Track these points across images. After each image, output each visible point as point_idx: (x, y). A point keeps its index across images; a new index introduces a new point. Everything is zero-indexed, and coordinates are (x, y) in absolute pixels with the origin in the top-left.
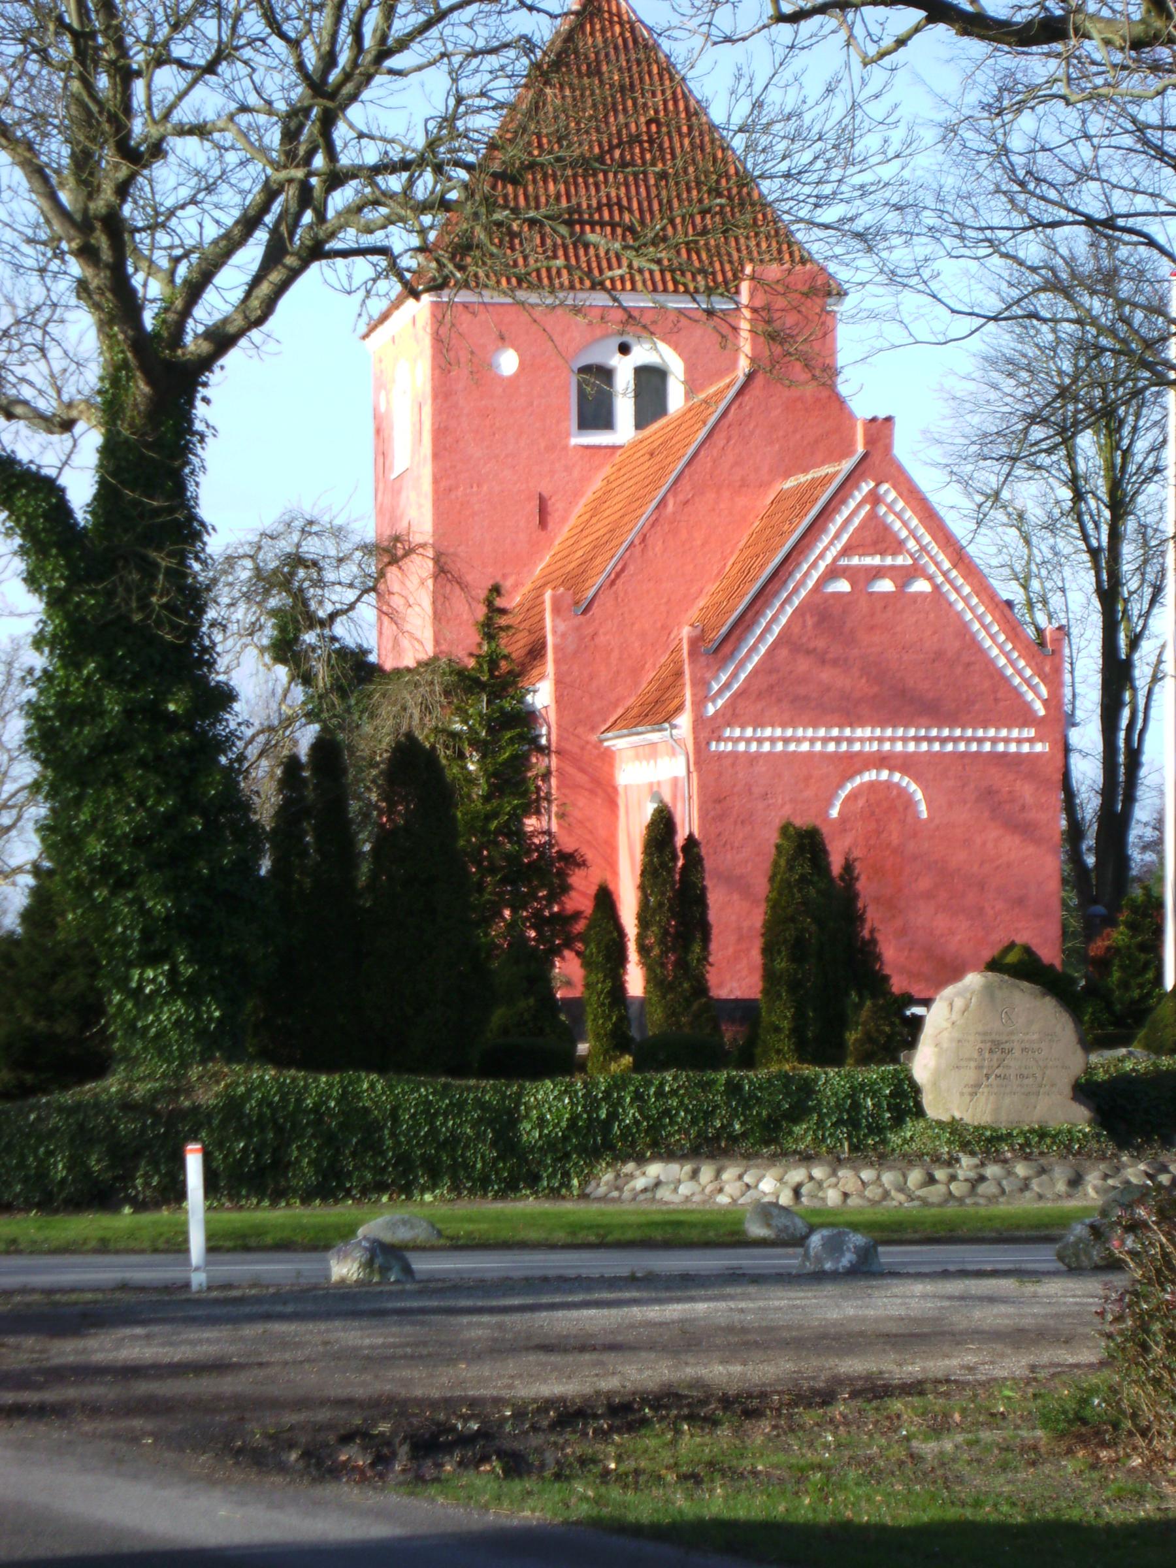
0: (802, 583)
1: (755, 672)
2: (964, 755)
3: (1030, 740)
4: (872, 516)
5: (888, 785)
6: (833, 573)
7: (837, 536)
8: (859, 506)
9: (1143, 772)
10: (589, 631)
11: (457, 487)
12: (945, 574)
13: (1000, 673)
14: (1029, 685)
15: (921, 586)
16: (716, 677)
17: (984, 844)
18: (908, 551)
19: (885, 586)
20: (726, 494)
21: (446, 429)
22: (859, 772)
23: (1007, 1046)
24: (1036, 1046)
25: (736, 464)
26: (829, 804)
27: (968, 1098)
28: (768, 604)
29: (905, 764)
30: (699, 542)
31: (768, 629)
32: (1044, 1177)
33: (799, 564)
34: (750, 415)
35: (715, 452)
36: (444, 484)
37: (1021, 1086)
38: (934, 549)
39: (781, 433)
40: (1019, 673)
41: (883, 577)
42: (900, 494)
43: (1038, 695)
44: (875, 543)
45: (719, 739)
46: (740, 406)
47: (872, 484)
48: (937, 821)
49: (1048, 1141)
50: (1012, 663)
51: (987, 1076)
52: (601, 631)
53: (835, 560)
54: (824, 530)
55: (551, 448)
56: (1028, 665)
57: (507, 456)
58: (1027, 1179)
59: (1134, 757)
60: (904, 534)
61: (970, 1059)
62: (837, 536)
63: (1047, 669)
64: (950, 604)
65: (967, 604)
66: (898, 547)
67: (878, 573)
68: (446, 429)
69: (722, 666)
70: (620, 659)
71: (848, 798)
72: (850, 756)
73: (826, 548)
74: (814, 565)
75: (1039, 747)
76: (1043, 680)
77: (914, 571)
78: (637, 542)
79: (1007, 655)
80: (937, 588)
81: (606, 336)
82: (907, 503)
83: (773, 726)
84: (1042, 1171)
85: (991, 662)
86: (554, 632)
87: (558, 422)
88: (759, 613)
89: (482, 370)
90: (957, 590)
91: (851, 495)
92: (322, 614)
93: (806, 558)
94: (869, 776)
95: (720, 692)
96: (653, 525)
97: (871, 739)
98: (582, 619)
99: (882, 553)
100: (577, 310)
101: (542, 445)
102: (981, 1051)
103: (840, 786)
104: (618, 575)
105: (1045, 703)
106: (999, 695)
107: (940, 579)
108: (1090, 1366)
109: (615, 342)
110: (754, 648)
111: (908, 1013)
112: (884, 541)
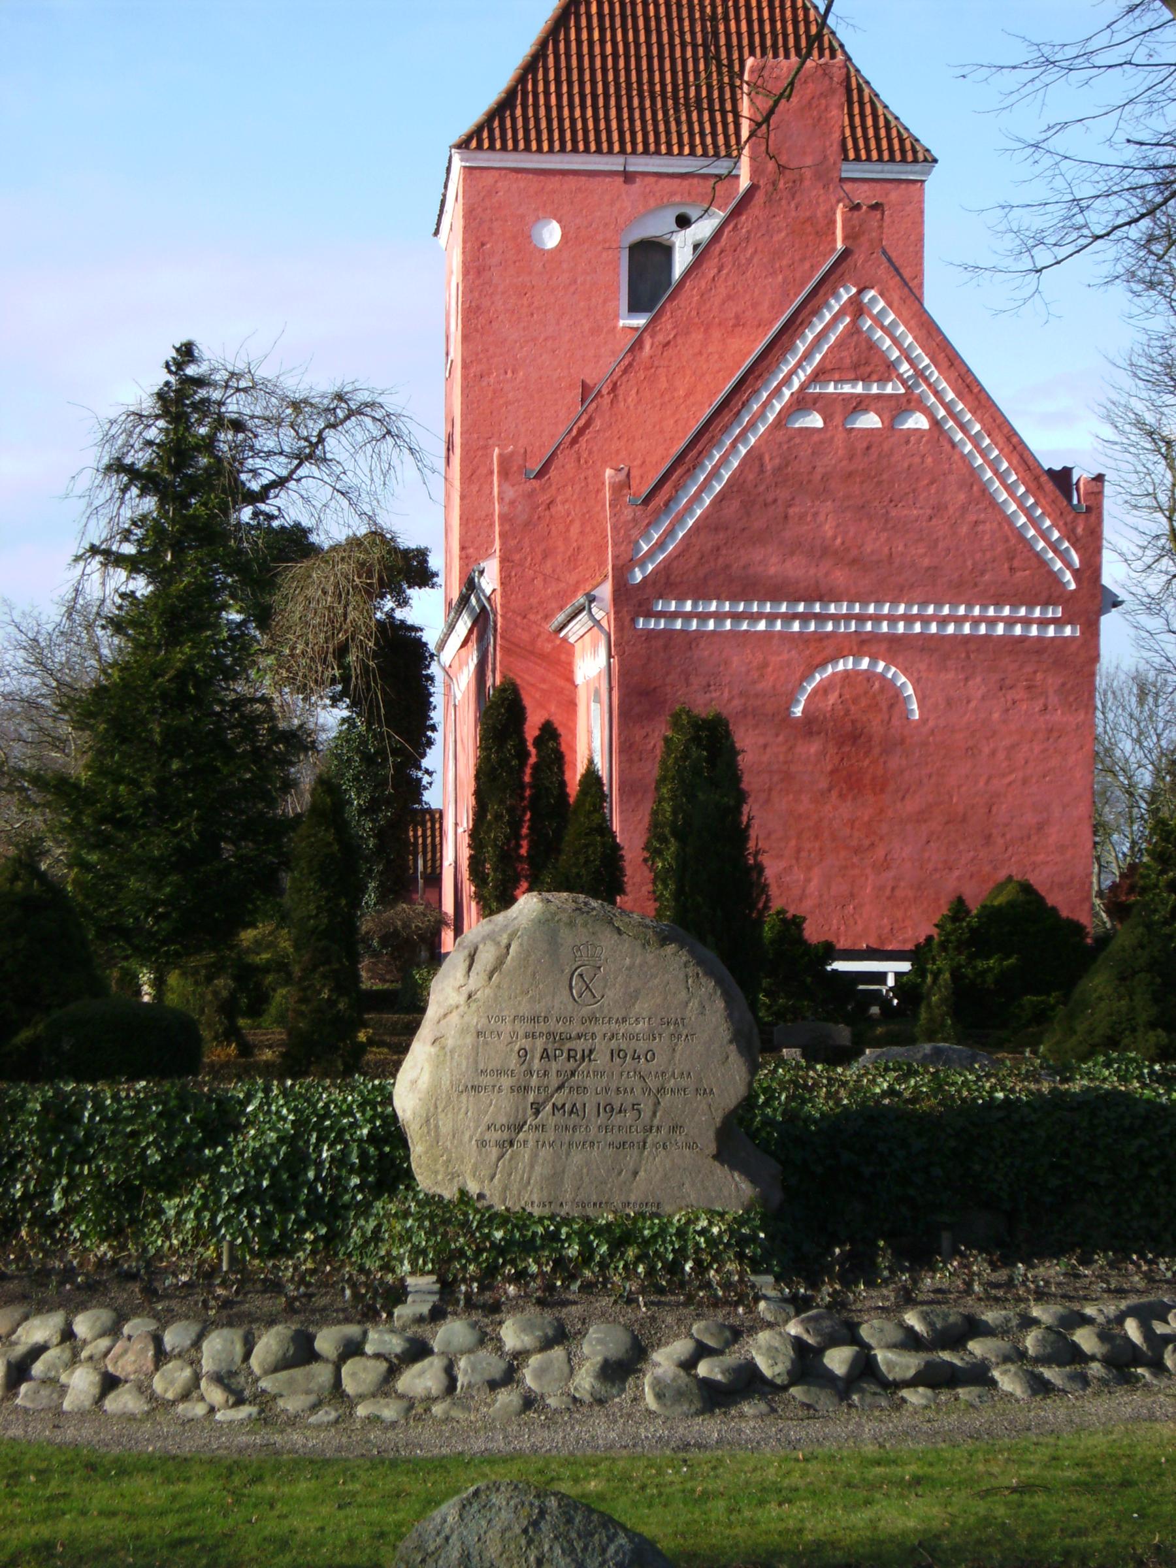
0: (761, 414)
1: (696, 528)
2: (967, 639)
3: (1057, 622)
4: (854, 330)
5: (869, 675)
6: (801, 402)
7: (807, 356)
8: (836, 318)
10: (544, 498)
11: (489, 374)
12: (948, 407)
13: (1019, 534)
14: (1056, 551)
15: (918, 421)
16: (645, 534)
17: (993, 753)
18: (900, 376)
19: (870, 421)
20: (716, 334)
21: (478, 307)
22: (834, 659)
23: (580, 1045)
24: (642, 1046)
25: (729, 297)
26: (792, 700)
27: (494, 1152)
28: (715, 442)
29: (894, 648)
30: (682, 393)
31: (715, 474)
32: (558, 1352)
33: (756, 392)
34: (748, 239)
35: (703, 284)
36: (474, 369)
38: (935, 375)
39: (785, 262)
40: (1044, 535)
41: (866, 410)
42: (890, 304)
43: (1068, 564)
44: (856, 366)
45: (649, 614)
46: (735, 228)
47: (854, 290)
48: (931, 723)
49: (631, 1253)
50: (1034, 522)
51: (537, 1110)
52: (559, 499)
53: (803, 387)
54: (790, 348)
55: (596, 331)
56: (1055, 525)
57: (546, 339)
58: (521, 1355)
60: (895, 354)
61: (500, 1072)
62: (807, 356)
63: (1079, 530)
64: (954, 445)
65: (977, 446)
66: (888, 370)
67: (860, 404)
68: (478, 307)
69: (653, 522)
70: (582, 533)
71: (815, 692)
72: (821, 638)
73: (793, 372)
74: (777, 392)
75: (1068, 631)
76: (1073, 545)
77: (908, 403)
78: (605, 391)
79: (1028, 512)
80: (936, 423)
81: (661, 206)
82: (898, 314)
83: (718, 598)
84: (559, 1336)
85: (1009, 520)
86: (501, 499)
87: (605, 302)
88: (705, 453)
89: (523, 241)
90: (963, 427)
91: (826, 304)
92: (255, 486)
93: (766, 384)
94: (845, 665)
95: (651, 554)
96: (625, 371)
97: (848, 617)
98: (536, 484)
99: (866, 379)
100: (628, 177)
101: (587, 327)
102: (523, 1054)
103: (807, 676)
104: (581, 432)
105: (1076, 573)
106: (1016, 564)
107: (941, 413)
109: (669, 218)
110: (697, 498)
111: (829, 968)
112: (867, 363)
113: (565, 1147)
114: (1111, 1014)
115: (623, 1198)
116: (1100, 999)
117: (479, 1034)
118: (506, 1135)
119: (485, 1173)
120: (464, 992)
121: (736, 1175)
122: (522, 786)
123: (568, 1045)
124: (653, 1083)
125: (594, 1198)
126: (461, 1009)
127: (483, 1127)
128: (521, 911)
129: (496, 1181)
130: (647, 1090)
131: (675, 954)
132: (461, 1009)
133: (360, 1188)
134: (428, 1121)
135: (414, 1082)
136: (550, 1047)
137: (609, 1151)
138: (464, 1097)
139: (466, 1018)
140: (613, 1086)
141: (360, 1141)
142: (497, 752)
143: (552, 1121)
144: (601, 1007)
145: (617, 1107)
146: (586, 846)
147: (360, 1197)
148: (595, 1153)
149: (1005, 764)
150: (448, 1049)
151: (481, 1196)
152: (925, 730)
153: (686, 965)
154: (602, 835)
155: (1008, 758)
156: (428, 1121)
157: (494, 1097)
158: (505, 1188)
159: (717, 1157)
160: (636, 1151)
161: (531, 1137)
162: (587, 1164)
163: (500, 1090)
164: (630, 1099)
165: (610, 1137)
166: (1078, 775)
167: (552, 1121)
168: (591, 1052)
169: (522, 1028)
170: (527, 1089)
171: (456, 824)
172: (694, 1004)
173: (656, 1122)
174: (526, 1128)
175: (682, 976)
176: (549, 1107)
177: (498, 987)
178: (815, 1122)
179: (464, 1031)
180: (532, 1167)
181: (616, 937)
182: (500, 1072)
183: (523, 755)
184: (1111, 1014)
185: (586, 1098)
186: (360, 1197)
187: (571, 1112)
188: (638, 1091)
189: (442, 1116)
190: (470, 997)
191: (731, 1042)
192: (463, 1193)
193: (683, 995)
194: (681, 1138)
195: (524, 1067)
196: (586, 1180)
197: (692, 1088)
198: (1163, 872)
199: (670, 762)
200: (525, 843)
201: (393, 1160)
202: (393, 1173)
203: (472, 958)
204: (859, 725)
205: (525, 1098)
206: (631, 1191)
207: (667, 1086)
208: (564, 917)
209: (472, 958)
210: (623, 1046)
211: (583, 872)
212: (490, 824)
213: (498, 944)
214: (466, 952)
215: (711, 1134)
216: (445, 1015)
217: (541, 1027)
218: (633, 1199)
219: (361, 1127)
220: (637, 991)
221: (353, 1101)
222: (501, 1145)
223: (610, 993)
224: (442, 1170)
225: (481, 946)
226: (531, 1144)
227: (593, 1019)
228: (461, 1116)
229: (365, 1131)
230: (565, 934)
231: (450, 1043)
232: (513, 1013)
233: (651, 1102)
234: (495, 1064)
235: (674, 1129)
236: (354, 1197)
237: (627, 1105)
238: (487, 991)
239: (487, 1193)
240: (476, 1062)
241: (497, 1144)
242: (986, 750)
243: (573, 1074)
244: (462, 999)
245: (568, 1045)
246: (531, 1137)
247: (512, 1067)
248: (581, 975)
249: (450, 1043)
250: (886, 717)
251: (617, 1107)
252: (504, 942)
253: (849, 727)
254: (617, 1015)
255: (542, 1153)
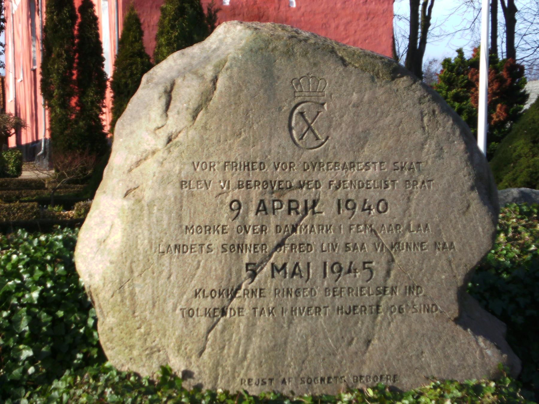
9: (430, 28)
17: (337, 27)
27: (204, 322)
37: (335, 292)
48: (302, 10)
59: (427, 20)
61: (209, 229)
108: (363, 98)
113: (286, 315)
114: (529, 167)
115: (355, 371)
116: (520, 156)
117: (182, 184)
118: (217, 303)
119: (192, 347)
120: (163, 135)
121: (481, 339)
122: (73, 37)
123: (289, 196)
124: (386, 238)
125: (322, 373)
126: (160, 155)
127: (190, 293)
128: (221, 41)
129: (205, 355)
130: (379, 245)
131: (408, 88)
132: (160, 155)
133: (31, 361)
134: (121, 287)
135: (103, 242)
136: (267, 198)
137: (338, 317)
138: (166, 258)
139: (167, 165)
140: (341, 243)
141: (30, 305)
142: (57, 15)
143: (271, 285)
144: (325, 150)
145: (345, 266)
146: (131, 64)
147: (31, 370)
148: (321, 320)
149: (343, 33)
150: (144, 203)
151: (187, 374)
152: (299, 13)
153: (420, 101)
154: (142, 57)
155: (345, 29)
156: (121, 287)
157: (202, 258)
158: (217, 364)
159: (457, 321)
160: (368, 318)
161: (248, 303)
162: (313, 333)
163: (209, 250)
164: (360, 257)
165: (338, 302)
166: (384, 39)
167: (271, 285)
168: (315, 203)
169: (234, 176)
170: (241, 247)
171: (15, 79)
172: (430, 146)
173: (390, 282)
174: (240, 293)
175: (416, 113)
176: (267, 268)
177: (205, 128)
178: (507, 270)
179: (164, 181)
180: (249, 338)
181: (341, 68)
182: (209, 229)
183: (73, 17)
184: (529, 167)
185: (310, 256)
186: (31, 370)
187: (294, 273)
188: (369, 247)
189: (138, 282)
190: (170, 140)
191: (472, 188)
192: (166, 371)
193: (419, 136)
194: (418, 301)
195: (237, 222)
196: (312, 351)
197: (430, 242)
198: (449, 90)
199: (166, 22)
200: (75, 72)
201: (67, 326)
202: (69, 340)
203: (169, 94)
204: (262, 10)
205: (239, 258)
206: (363, 362)
207: (401, 240)
208: (280, 45)
209: (169, 94)
210: (351, 196)
211: (129, 81)
212: (54, 60)
213: (202, 77)
214: (161, 89)
215: (452, 295)
216: (138, 163)
217: (256, 175)
218: (365, 372)
219: (30, 291)
220: (366, 132)
221: (19, 261)
222: (211, 313)
223: (335, 134)
224: (139, 344)
225: (179, 81)
226: (247, 312)
227: (316, 164)
228: (162, 281)
229: (35, 295)
230: (281, 63)
231: (148, 195)
232: (224, 158)
233: (384, 260)
234: (201, 220)
235: (411, 289)
236: (25, 371)
237: (358, 263)
238: (191, 132)
239: (194, 369)
240: (180, 217)
241: (206, 312)
242: (333, 25)
243: (294, 230)
244: (160, 143)
245: (289, 196)
246: (248, 303)
247: (224, 222)
248: (301, 114)
249: (148, 195)
250: (277, 6)
251: (345, 266)
252: (209, 73)
253: (256, 11)
254: (345, 159)
255: (260, 322)
